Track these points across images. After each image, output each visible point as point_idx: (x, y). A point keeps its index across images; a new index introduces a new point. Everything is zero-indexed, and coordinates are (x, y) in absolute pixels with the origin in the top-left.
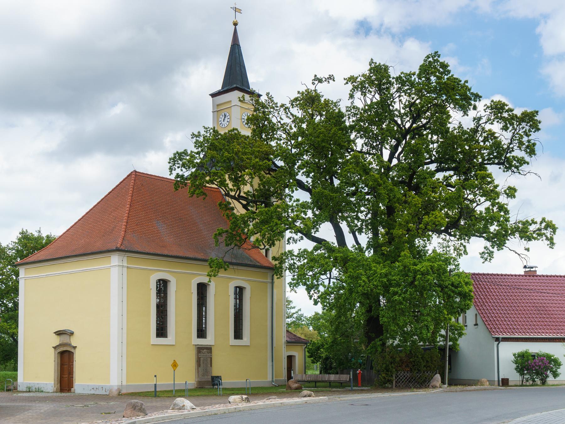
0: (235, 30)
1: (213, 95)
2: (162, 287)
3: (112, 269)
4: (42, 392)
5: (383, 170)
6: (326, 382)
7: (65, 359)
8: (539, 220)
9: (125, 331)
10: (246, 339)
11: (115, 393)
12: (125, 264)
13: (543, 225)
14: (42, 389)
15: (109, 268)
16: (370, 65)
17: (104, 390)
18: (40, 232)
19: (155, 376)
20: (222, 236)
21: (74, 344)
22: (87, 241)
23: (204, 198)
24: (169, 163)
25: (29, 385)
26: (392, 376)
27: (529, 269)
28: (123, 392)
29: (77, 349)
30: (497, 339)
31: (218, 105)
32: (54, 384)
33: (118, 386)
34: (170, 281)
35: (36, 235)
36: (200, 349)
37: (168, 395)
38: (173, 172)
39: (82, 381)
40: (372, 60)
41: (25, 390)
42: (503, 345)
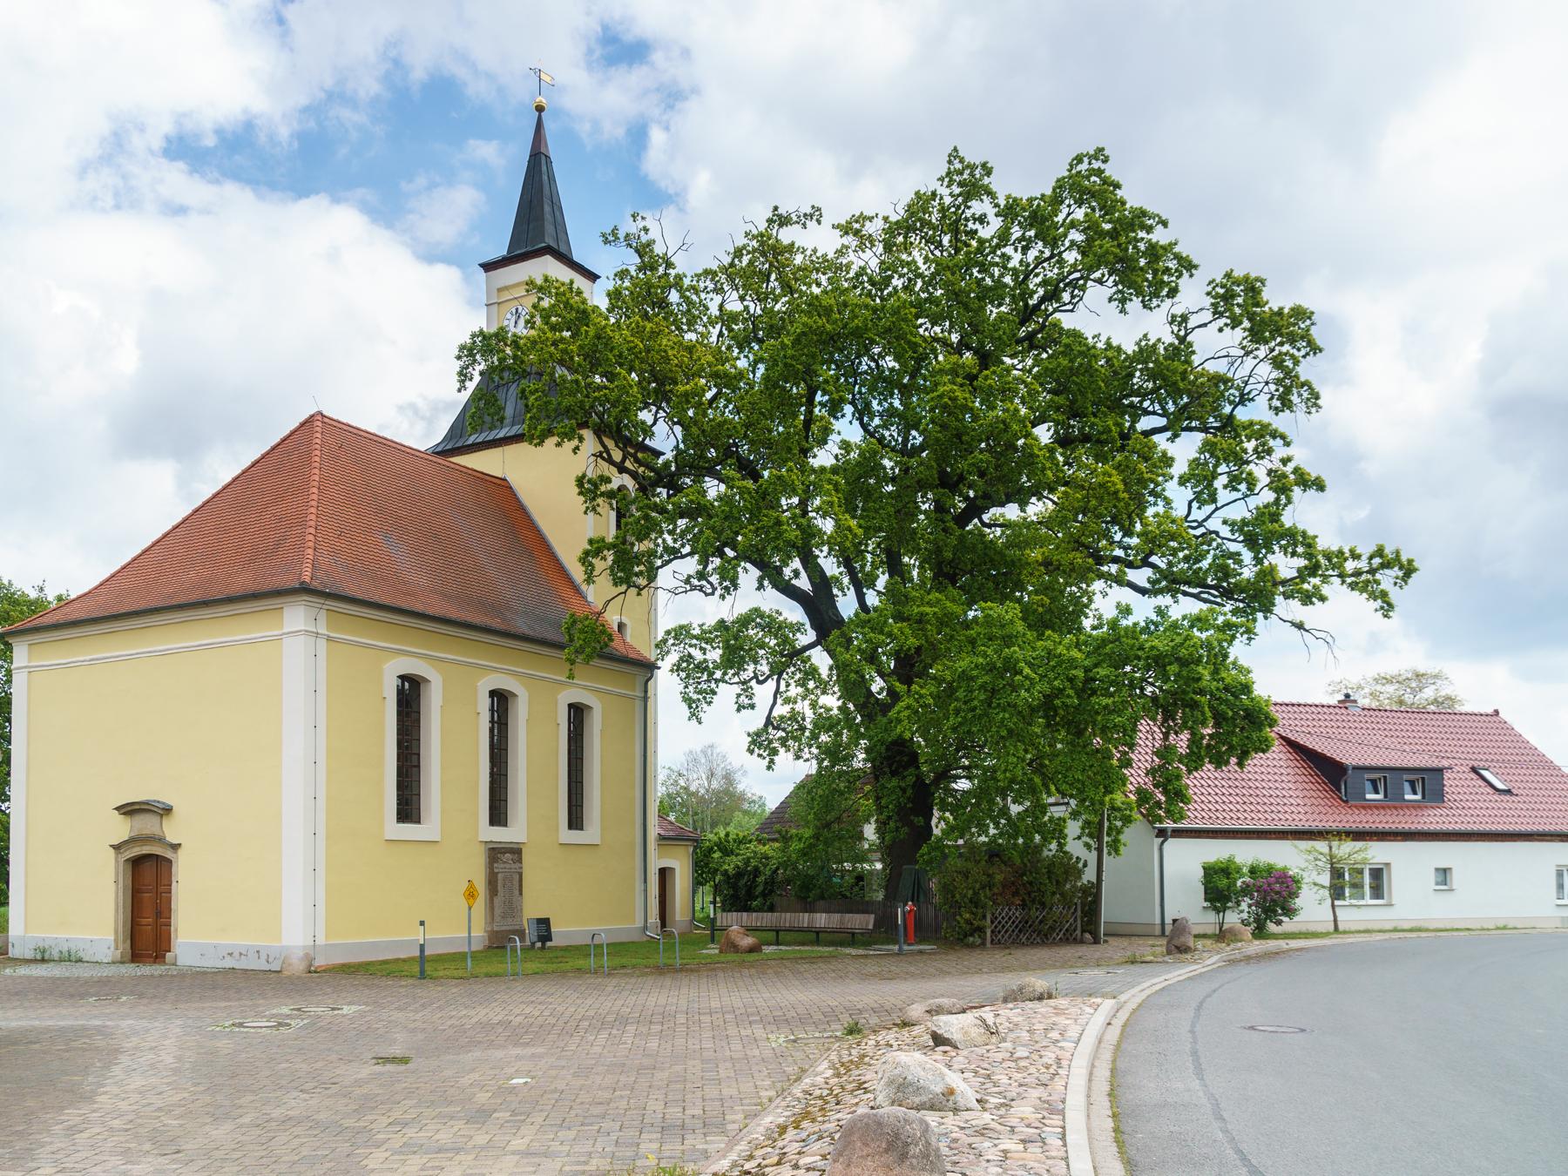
0: (540, 119)
2: (410, 695)
3: (287, 641)
4: (80, 960)
6: (801, 930)
7: (147, 879)
8: (1365, 550)
9: (322, 802)
10: (591, 833)
11: (298, 966)
12: (323, 631)
13: (1377, 561)
14: (81, 954)
15: (279, 638)
16: (950, 162)
17: (264, 957)
18: (41, 589)
19: (422, 923)
20: (604, 558)
21: (171, 838)
22: (206, 572)
23: (577, 448)
24: (459, 358)
25: (41, 945)
26: (984, 917)
28: (317, 963)
29: (180, 852)
30: (1162, 833)
31: (499, 290)
32: (116, 941)
33: (304, 947)
34: (427, 681)
35: (33, 595)
36: (496, 853)
37: (455, 973)
38: (468, 384)
39: (196, 931)
40: (955, 149)
41: (29, 955)
42: (1172, 845)
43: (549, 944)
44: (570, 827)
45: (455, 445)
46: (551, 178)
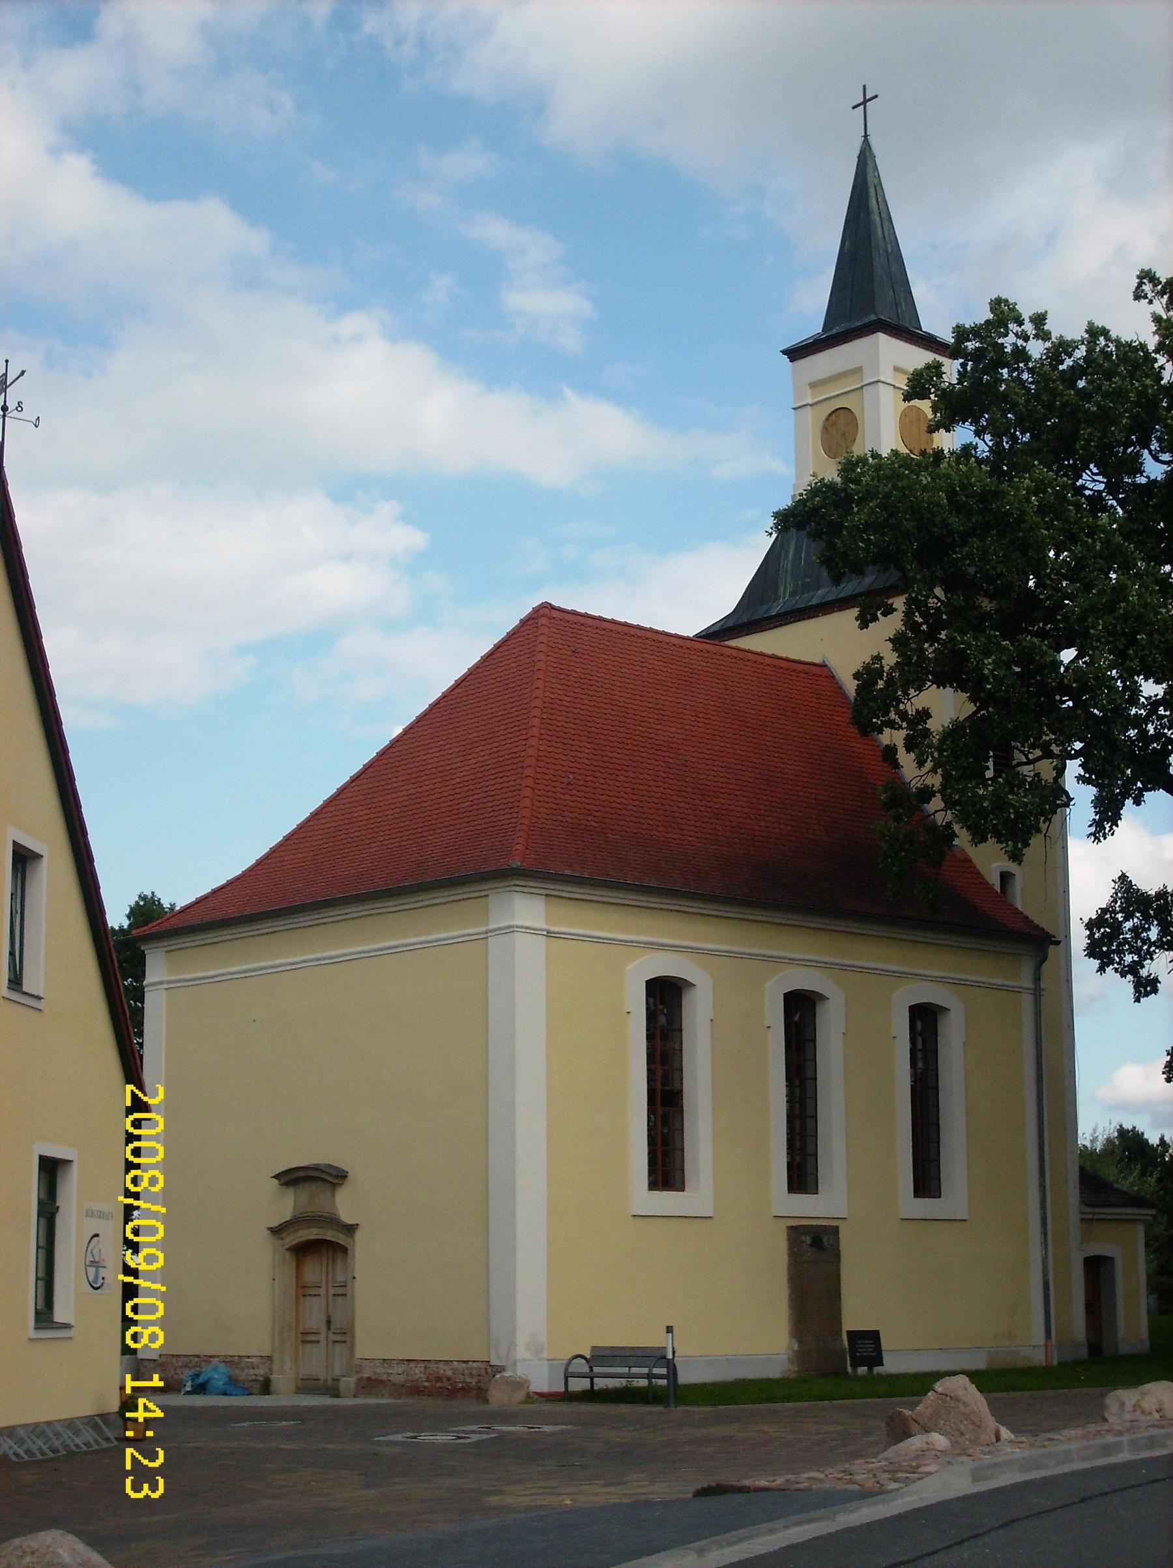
1: (795, 353)
5: (1078, 745)
10: (956, 1197)
15: (485, 936)
21: (347, 1218)
22: (409, 834)
27: (634, 1370)
29: (359, 1235)
44: (653, 1185)
45: (759, 608)
46: (879, 185)
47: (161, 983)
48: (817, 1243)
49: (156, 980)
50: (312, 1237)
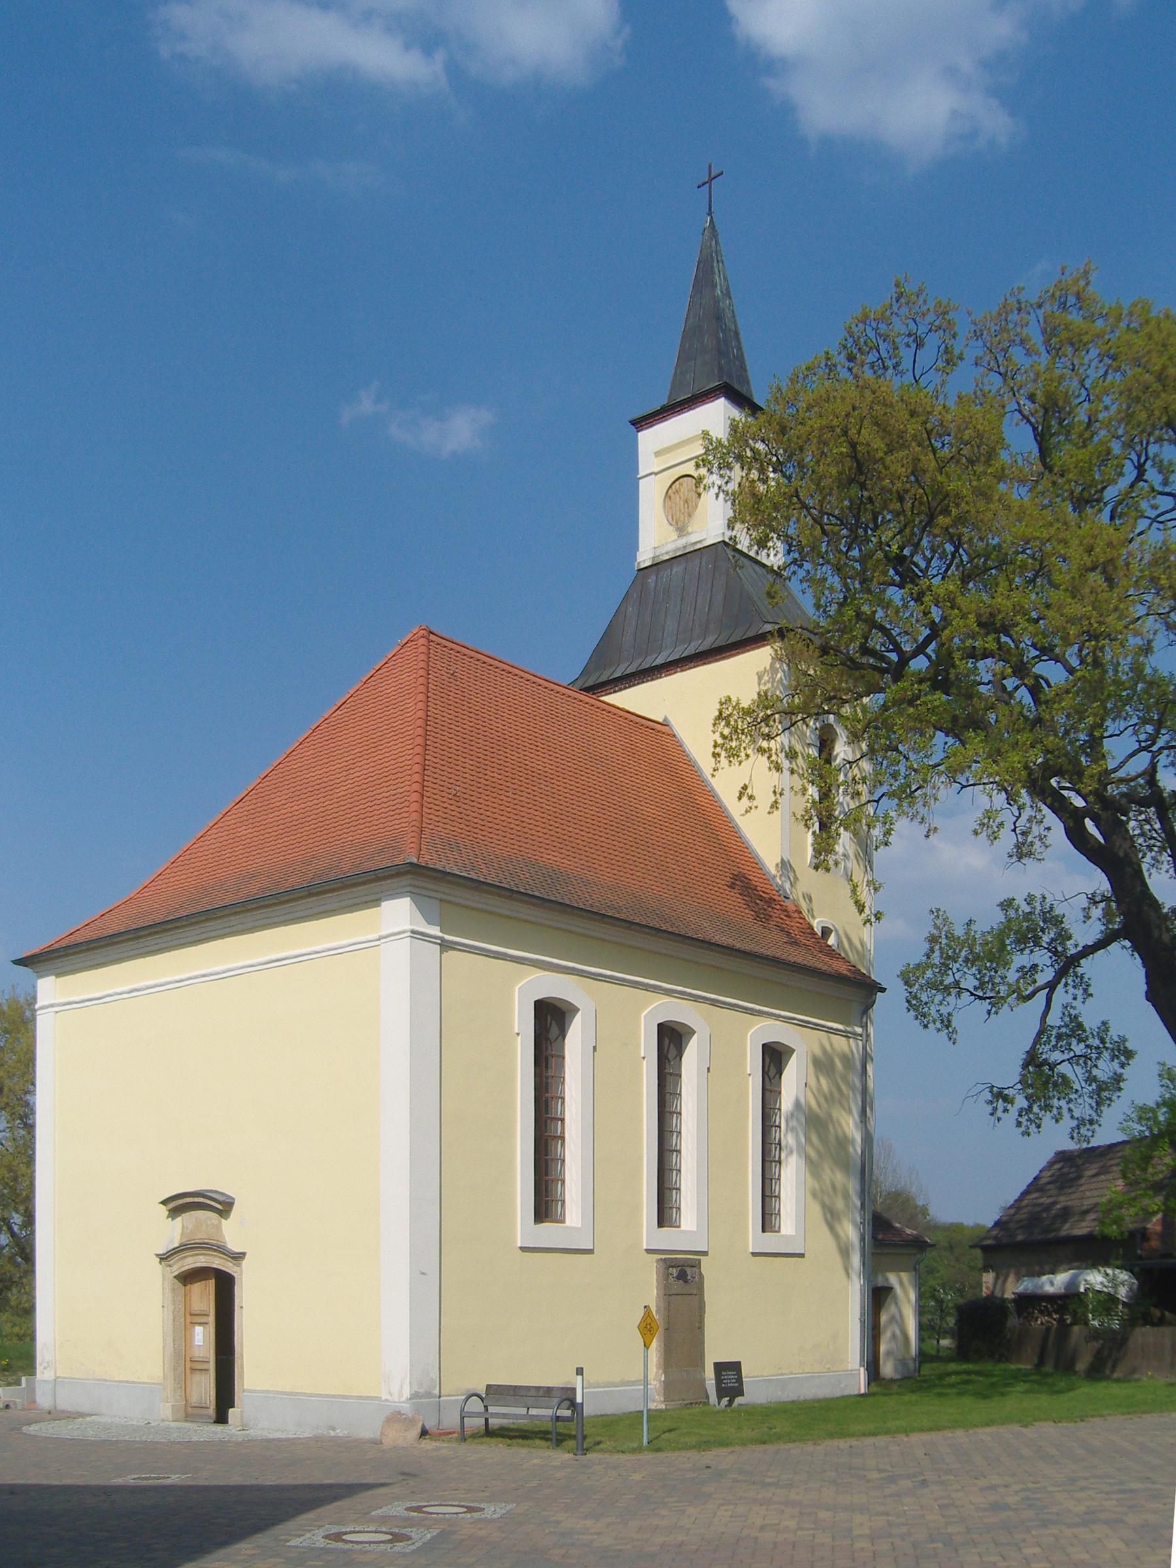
21: (234, 1246)
29: (245, 1263)
34: (576, 1010)
43: (739, 1400)
47: (52, 1006)
48: (682, 1276)
49: (46, 1003)
50: (199, 1265)
